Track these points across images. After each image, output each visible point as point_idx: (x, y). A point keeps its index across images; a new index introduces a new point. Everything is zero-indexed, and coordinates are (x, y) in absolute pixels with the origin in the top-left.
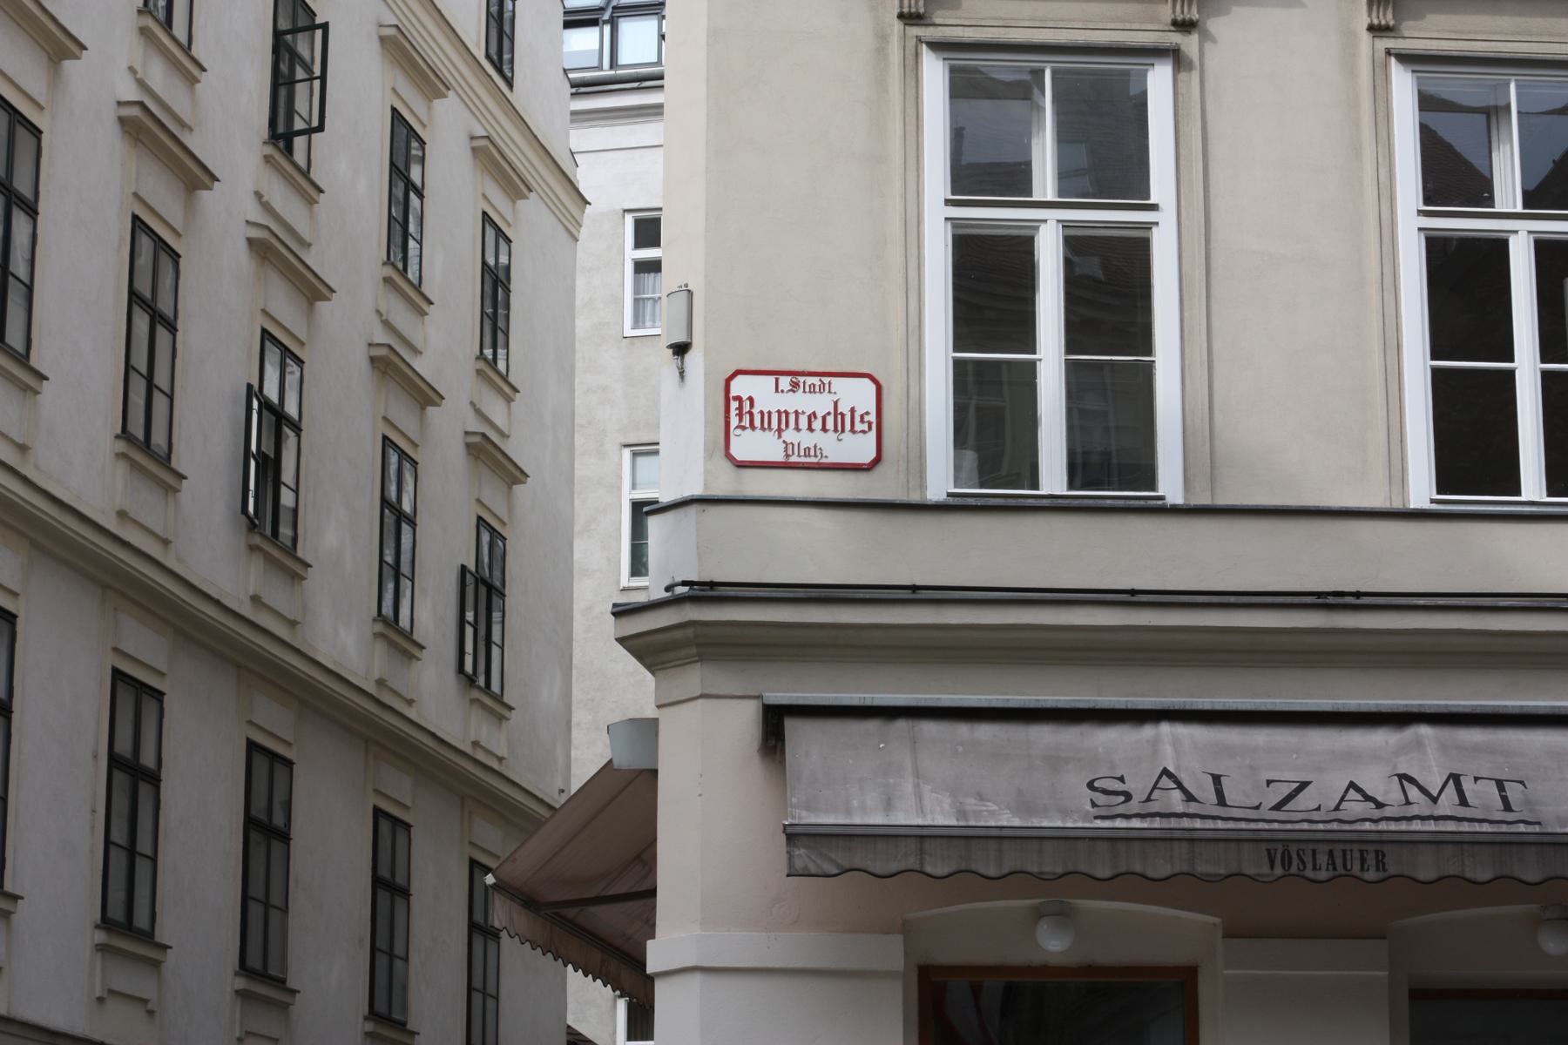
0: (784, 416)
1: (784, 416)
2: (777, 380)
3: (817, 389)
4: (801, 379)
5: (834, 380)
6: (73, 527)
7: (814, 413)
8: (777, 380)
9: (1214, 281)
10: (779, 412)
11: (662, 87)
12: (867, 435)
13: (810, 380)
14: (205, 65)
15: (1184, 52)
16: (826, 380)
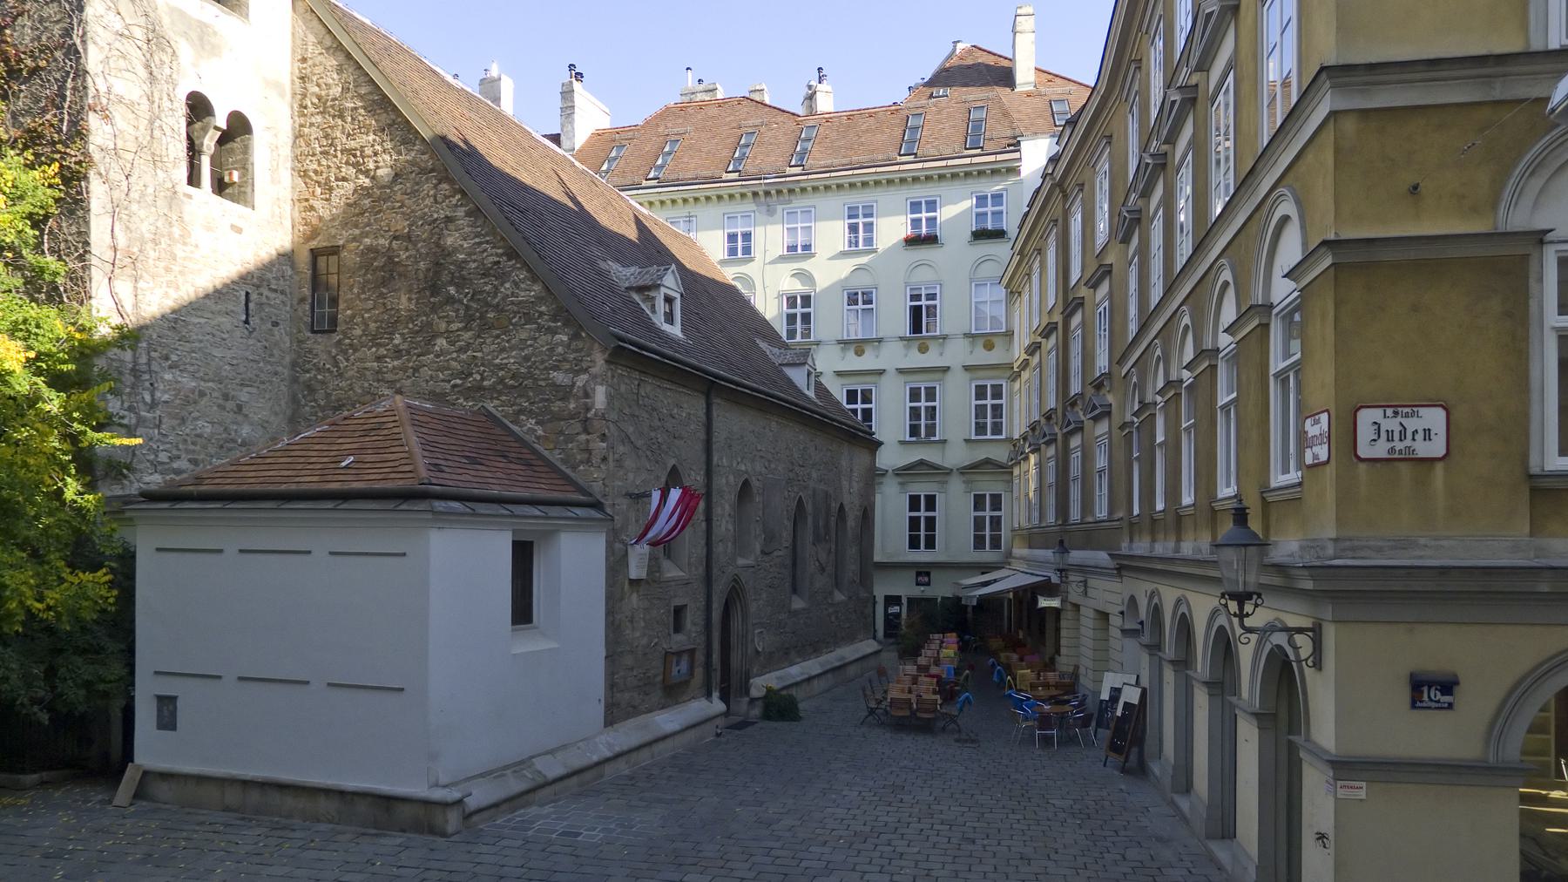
0: (1427, 432)
1: (1427, 432)
2: (1385, 411)
3: (1410, 415)
4: (1400, 409)
5: (1421, 409)
6: (1188, 291)
7: (1416, 431)
8: (1385, 411)
9: (175, 555)
10: (1425, 430)
11: (1450, 706)
12: (1378, 442)
13: (1406, 410)
14: (333, 557)
15: (1048, 152)
16: (1415, 409)
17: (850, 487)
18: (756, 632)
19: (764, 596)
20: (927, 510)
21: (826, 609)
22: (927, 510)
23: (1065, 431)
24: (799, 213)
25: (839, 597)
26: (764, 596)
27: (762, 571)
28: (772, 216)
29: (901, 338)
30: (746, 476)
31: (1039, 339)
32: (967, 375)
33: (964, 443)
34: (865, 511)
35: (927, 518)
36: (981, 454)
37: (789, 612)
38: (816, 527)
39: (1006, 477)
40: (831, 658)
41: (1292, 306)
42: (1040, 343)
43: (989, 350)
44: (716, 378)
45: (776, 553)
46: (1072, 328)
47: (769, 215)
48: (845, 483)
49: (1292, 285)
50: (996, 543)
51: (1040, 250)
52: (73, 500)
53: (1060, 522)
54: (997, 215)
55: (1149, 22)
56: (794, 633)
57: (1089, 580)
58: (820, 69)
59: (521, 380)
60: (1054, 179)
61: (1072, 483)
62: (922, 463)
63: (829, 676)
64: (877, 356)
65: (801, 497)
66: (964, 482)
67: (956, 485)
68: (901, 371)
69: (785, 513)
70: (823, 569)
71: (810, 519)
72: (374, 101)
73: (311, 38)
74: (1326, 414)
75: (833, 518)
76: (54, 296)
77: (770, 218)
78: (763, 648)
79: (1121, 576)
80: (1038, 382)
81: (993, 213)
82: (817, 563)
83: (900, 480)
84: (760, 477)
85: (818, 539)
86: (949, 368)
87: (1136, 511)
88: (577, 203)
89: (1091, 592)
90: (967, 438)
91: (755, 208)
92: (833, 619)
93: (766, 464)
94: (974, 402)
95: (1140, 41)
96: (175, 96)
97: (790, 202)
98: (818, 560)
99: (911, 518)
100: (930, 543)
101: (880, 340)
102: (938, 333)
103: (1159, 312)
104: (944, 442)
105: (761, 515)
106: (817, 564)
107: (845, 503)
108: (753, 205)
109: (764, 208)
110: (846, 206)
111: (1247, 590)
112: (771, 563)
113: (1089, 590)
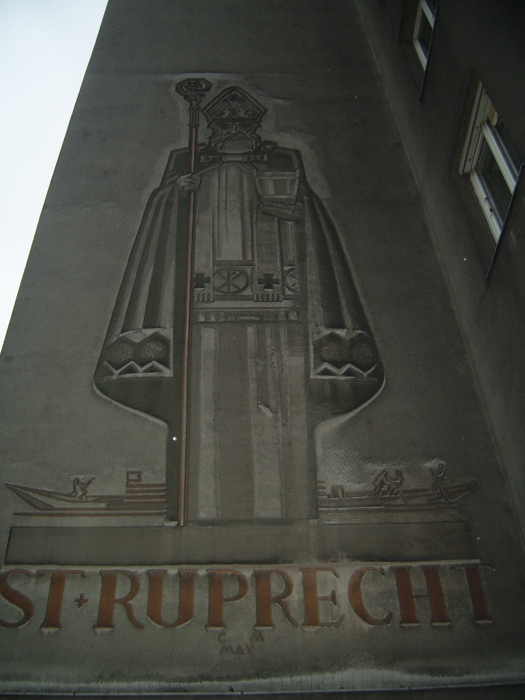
40: (453, 562)
41: (184, 424)
44: (175, 691)
52: (275, 374)
59: (258, 598)
72: (215, 688)
73: (200, 519)
74: (130, 475)
76: (210, 87)
80: (214, 221)
87: (512, 184)
88: (95, 497)
95: (188, 427)
96: (187, 525)
103: (194, 262)
111: (425, 592)
112: (367, 358)
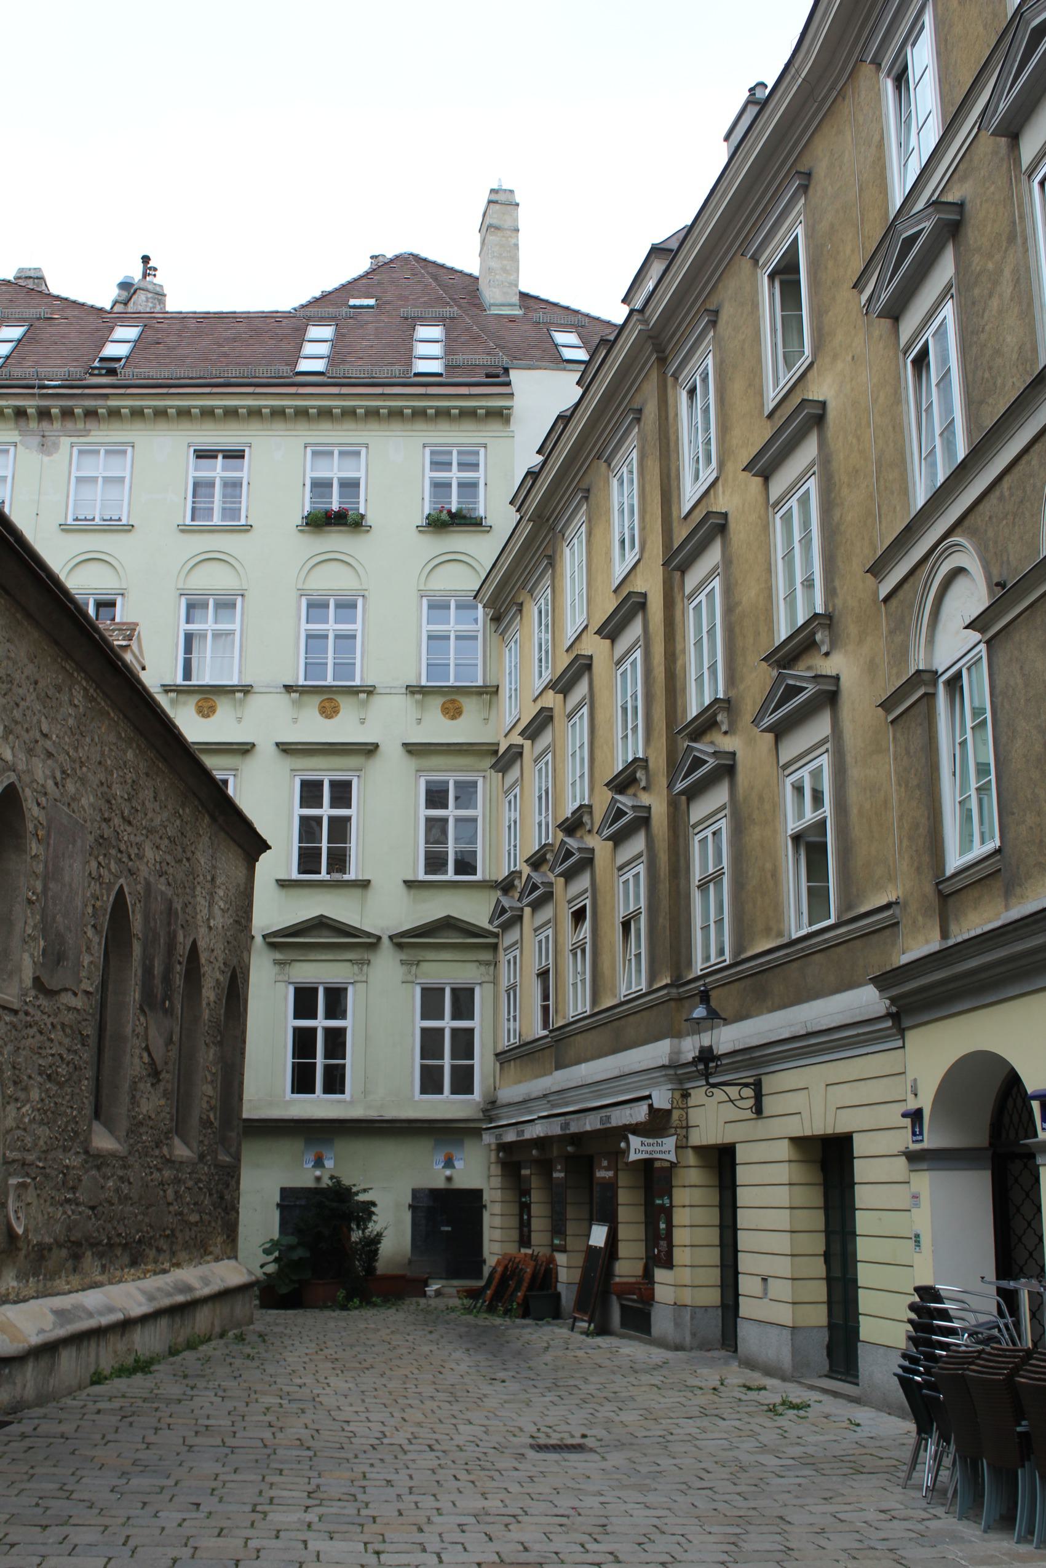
17: (211, 915)
18: (13, 1181)
19: (35, 1095)
20: (329, 1015)
21: (159, 1170)
22: (329, 1015)
23: (680, 786)
24: (102, 452)
25: (181, 1151)
26: (35, 1095)
27: (33, 1031)
28: (49, 454)
29: (288, 688)
30: (13, 777)
31: (519, 740)
32: (411, 764)
33: (402, 889)
34: (233, 978)
35: (328, 1031)
36: (434, 908)
37: (87, 1152)
38: (148, 971)
39: (487, 956)
42: (522, 746)
43: (453, 718)
45: (67, 999)
46: (688, 590)
47: (43, 452)
48: (202, 902)
49: (975, 636)
50: (463, 1082)
51: (588, 490)
53: (667, 980)
54: (469, 488)
55: (570, 434)
56: (93, 1208)
57: (764, 1078)
58: (146, 259)
60: (646, 322)
61: (696, 896)
62: (322, 924)
63: (164, 1322)
64: (239, 720)
65: (121, 887)
66: (402, 962)
67: (386, 962)
68: (286, 749)
69: (90, 910)
70: (155, 1074)
71: (137, 949)
75: (178, 967)
77: (46, 459)
78: (26, 1230)
79: (902, 1032)
81: (461, 485)
82: (145, 1055)
83: (278, 956)
84: (43, 800)
85: (149, 1002)
86: (376, 746)
89: (770, 1105)
90: (410, 878)
91: (17, 439)
92: (170, 1193)
93: (58, 775)
94: (424, 812)
97: (86, 433)
98: (147, 1049)
99: (297, 1031)
100: (335, 1082)
101: (246, 690)
102: (357, 682)
104: (365, 884)
105: (39, 889)
106: (146, 1059)
107: (202, 944)
108: (17, 433)
109: (35, 440)
110: (192, 449)
113: (766, 1101)
